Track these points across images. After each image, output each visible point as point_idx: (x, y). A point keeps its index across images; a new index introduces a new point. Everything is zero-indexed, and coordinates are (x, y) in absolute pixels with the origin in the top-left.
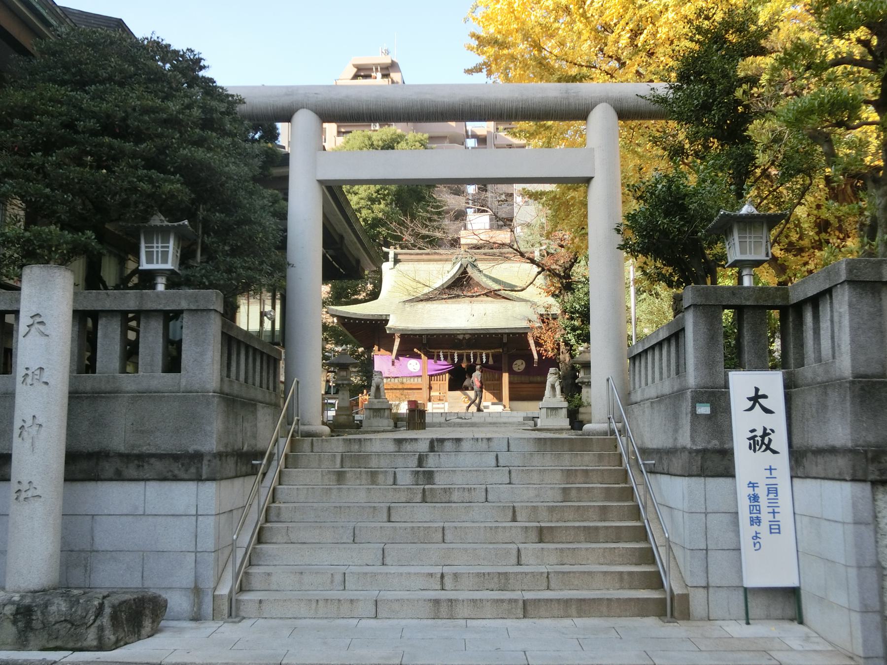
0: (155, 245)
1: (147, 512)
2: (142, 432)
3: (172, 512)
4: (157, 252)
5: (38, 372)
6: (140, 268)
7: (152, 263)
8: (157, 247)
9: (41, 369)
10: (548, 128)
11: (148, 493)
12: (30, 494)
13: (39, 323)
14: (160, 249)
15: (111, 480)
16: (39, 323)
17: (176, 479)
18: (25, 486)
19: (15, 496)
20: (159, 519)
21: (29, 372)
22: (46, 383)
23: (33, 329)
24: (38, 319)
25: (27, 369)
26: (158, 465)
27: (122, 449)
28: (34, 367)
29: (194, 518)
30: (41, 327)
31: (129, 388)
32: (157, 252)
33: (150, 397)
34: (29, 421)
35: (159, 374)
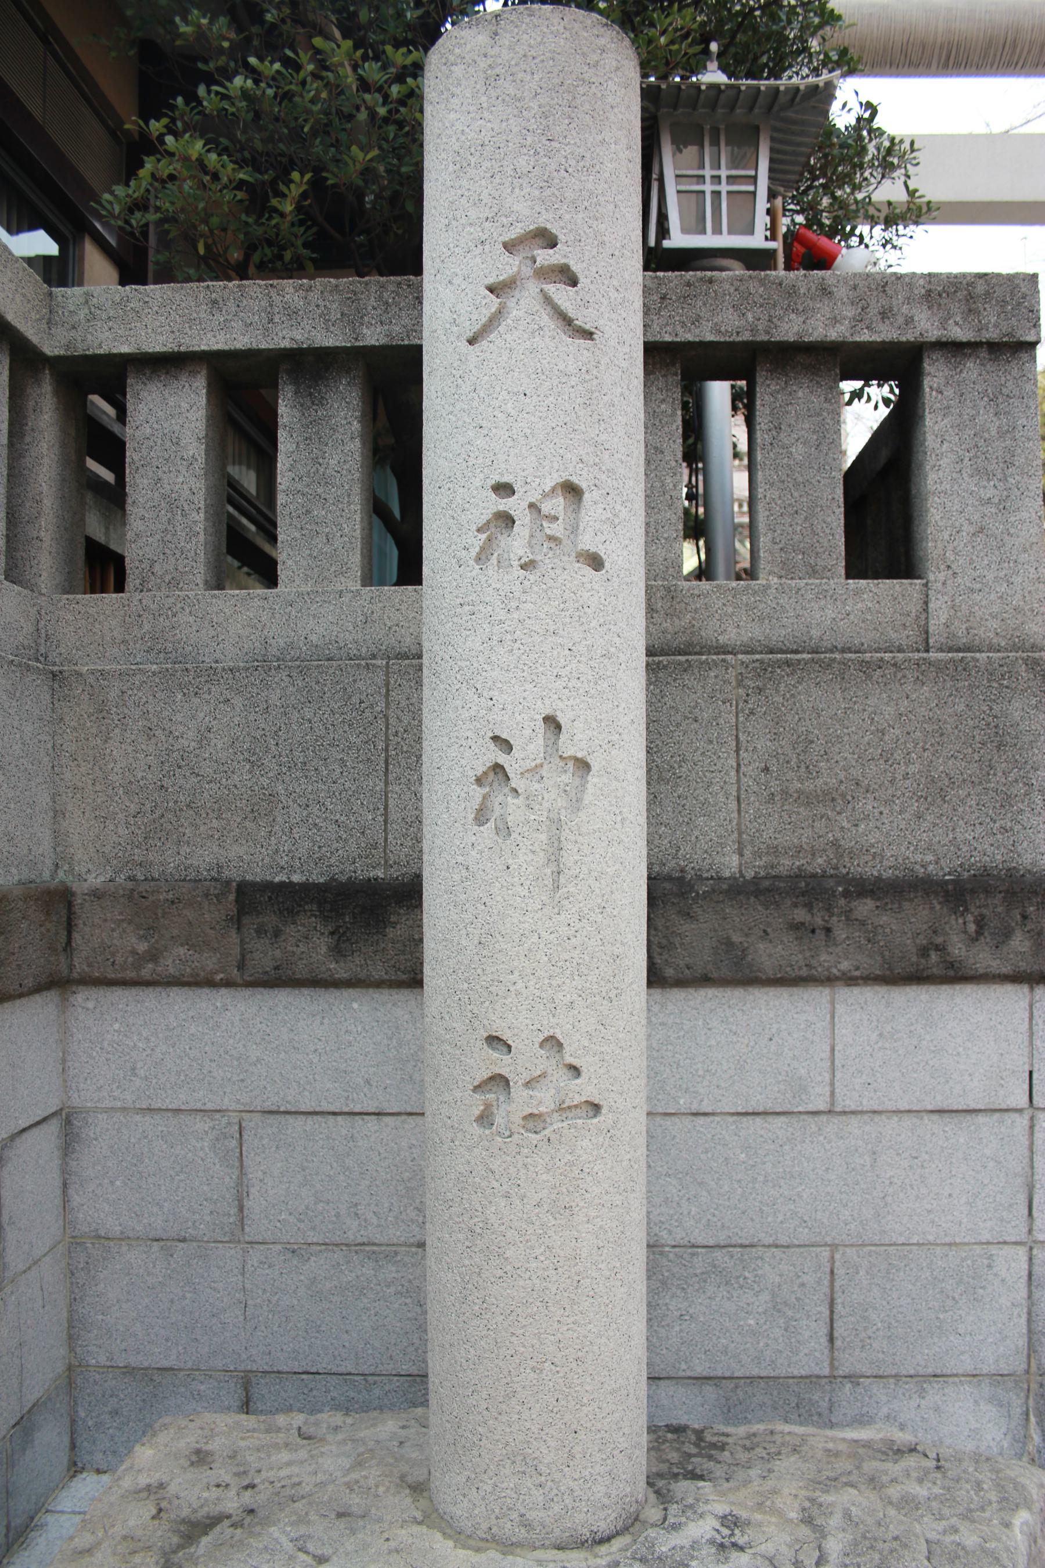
0: (708, 173)
1: (846, 1101)
2: (806, 799)
3: (940, 1103)
4: (716, 194)
5: (557, 505)
6: (666, 244)
7: (703, 232)
8: (717, 179)
9: (572, 491)
10: (673, 415)
11: (844, 1032)
12: (544, 1099)
13: (545, 274)
14: (724, 188)
15: (705, 980)
16: (545, 274)
17: (956, 975)
18: (526, 1059)
19: (476, 1104)
20: (890, 1126)
21: (513, 505)
22: (596, 562)
23: (525, 303)
24: (545, 257)
25: (504, 489)
26: (905, 926)
27: (730, 864)
28: (536, 481)
29: (1022, 1122)
30: (562, 295)
31: (730, 636)
32: (716, 194)
33: (788, 663)
34: (530, 745)
35: (838, 581)
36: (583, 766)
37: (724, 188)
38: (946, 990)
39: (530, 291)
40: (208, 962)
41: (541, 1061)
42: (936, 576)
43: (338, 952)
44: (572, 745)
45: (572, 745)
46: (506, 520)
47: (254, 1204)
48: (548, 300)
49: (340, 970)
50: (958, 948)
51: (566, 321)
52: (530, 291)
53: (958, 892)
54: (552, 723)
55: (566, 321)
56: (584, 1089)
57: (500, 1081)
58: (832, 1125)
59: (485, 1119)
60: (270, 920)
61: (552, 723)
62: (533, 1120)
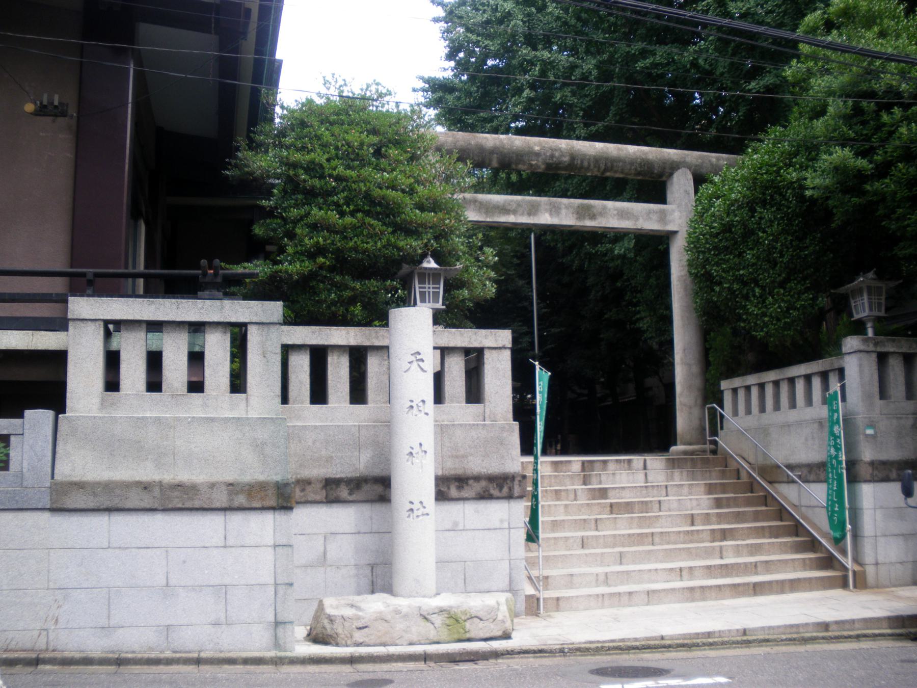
1: (467, 527)
5: (421, 404)
9: (423, 401)
13: (418, 360)
16: (418, 360)
21: (414, 404)
24: (419, 357)
25: (412, 401)
28: (417, 401)
30: (420, 363)
34: (417, 449)
36: (425, 452)
37: (426, 290)
38: (489, 501)
39: (415, 364)
40: (318, 498)
41: (419, 506)
42: (487, 403)
43: (350, 494)
44: (424, 448)
45: (424, 448)
46: (412, 407)
47: (328, 556)
48: (419, 365)
49: (350, 498)
50: (492, 491)
51: (422, 369)
52: (415, 364)
53: (491, 479)
54: (421, 445)
55: (422, 369)
56: (425, 511)
57: (412, 510)
58: (464, 533)
59: (409, 516)
60: (334, 487)
61: (421, 445)
62: (418, 516)
